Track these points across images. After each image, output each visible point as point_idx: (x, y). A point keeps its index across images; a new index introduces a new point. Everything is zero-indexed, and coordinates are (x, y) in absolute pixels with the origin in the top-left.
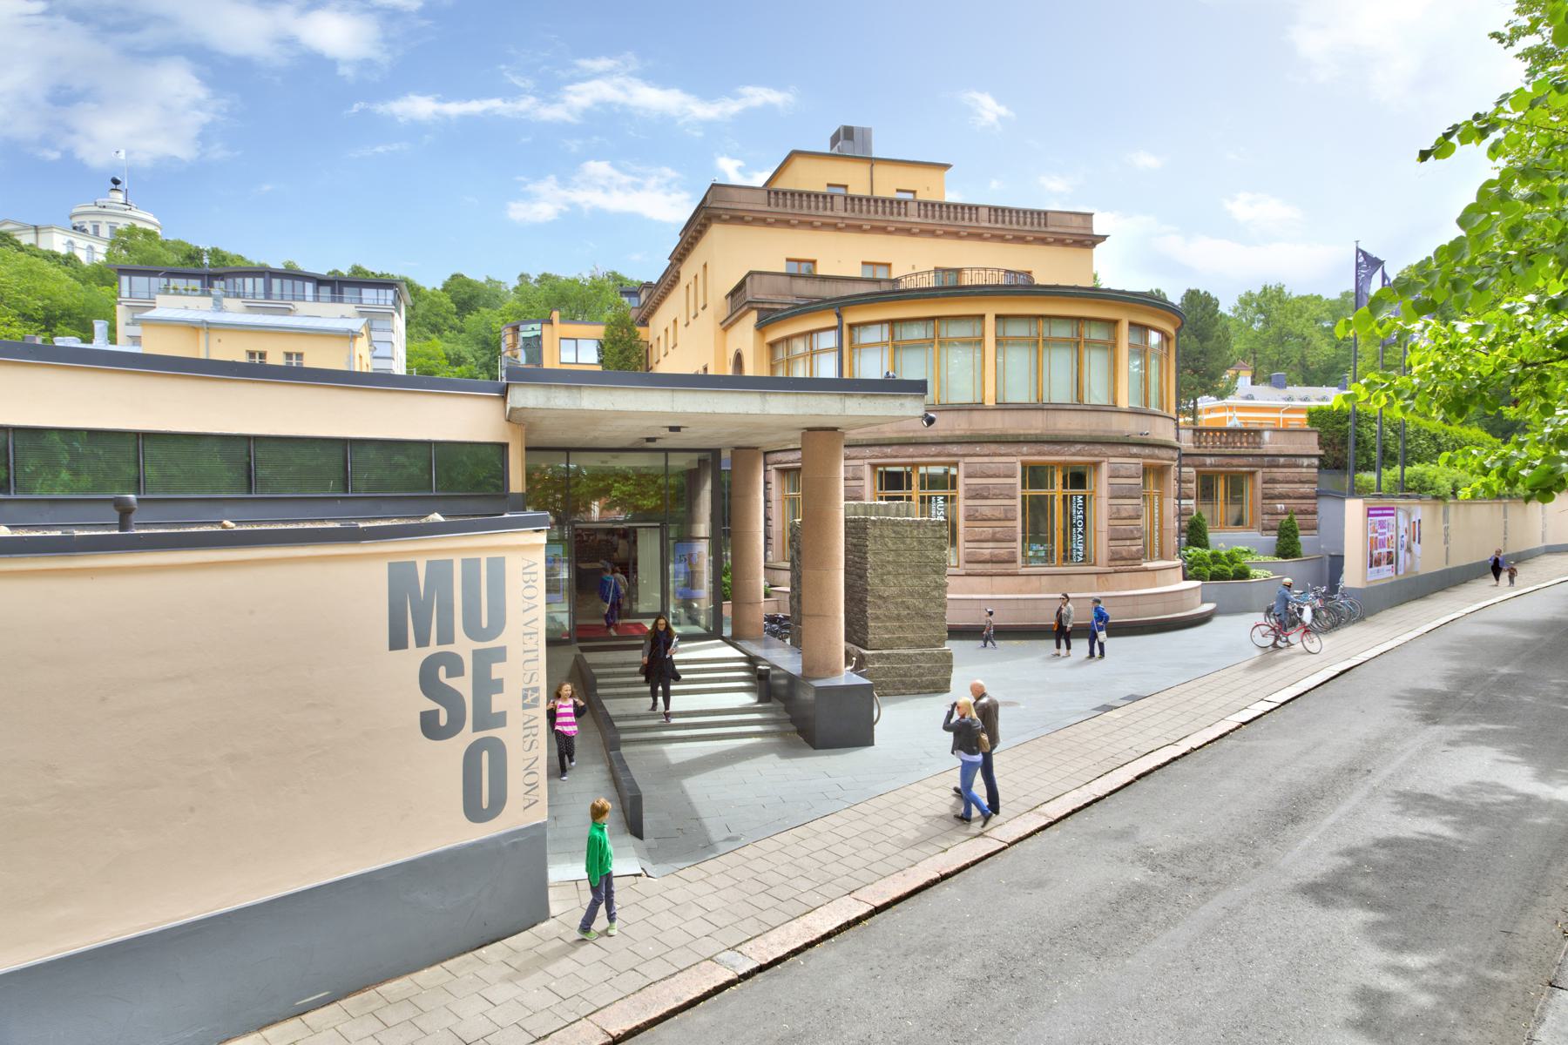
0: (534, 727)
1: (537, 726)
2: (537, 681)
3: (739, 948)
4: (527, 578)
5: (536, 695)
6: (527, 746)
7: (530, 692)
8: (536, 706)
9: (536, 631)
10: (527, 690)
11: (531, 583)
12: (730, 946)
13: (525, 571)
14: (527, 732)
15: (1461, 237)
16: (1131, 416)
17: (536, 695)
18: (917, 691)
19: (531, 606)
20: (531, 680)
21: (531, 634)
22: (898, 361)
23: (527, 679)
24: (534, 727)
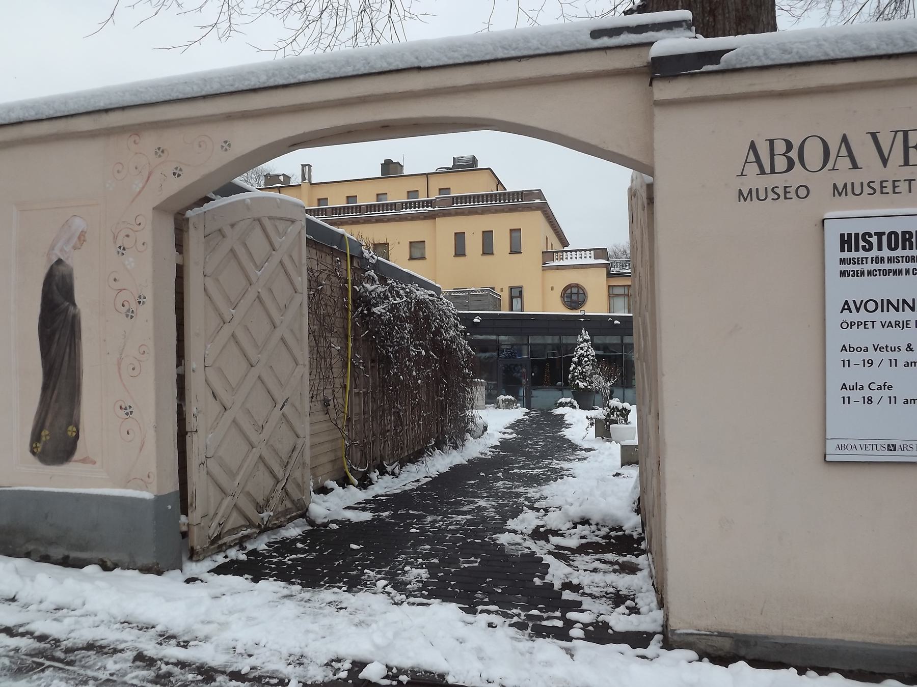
1: (771, 142)
4: (781, 163)
9: (900, 136)
11: (794, 154)
13: (767, 169)
19: (844, 151)
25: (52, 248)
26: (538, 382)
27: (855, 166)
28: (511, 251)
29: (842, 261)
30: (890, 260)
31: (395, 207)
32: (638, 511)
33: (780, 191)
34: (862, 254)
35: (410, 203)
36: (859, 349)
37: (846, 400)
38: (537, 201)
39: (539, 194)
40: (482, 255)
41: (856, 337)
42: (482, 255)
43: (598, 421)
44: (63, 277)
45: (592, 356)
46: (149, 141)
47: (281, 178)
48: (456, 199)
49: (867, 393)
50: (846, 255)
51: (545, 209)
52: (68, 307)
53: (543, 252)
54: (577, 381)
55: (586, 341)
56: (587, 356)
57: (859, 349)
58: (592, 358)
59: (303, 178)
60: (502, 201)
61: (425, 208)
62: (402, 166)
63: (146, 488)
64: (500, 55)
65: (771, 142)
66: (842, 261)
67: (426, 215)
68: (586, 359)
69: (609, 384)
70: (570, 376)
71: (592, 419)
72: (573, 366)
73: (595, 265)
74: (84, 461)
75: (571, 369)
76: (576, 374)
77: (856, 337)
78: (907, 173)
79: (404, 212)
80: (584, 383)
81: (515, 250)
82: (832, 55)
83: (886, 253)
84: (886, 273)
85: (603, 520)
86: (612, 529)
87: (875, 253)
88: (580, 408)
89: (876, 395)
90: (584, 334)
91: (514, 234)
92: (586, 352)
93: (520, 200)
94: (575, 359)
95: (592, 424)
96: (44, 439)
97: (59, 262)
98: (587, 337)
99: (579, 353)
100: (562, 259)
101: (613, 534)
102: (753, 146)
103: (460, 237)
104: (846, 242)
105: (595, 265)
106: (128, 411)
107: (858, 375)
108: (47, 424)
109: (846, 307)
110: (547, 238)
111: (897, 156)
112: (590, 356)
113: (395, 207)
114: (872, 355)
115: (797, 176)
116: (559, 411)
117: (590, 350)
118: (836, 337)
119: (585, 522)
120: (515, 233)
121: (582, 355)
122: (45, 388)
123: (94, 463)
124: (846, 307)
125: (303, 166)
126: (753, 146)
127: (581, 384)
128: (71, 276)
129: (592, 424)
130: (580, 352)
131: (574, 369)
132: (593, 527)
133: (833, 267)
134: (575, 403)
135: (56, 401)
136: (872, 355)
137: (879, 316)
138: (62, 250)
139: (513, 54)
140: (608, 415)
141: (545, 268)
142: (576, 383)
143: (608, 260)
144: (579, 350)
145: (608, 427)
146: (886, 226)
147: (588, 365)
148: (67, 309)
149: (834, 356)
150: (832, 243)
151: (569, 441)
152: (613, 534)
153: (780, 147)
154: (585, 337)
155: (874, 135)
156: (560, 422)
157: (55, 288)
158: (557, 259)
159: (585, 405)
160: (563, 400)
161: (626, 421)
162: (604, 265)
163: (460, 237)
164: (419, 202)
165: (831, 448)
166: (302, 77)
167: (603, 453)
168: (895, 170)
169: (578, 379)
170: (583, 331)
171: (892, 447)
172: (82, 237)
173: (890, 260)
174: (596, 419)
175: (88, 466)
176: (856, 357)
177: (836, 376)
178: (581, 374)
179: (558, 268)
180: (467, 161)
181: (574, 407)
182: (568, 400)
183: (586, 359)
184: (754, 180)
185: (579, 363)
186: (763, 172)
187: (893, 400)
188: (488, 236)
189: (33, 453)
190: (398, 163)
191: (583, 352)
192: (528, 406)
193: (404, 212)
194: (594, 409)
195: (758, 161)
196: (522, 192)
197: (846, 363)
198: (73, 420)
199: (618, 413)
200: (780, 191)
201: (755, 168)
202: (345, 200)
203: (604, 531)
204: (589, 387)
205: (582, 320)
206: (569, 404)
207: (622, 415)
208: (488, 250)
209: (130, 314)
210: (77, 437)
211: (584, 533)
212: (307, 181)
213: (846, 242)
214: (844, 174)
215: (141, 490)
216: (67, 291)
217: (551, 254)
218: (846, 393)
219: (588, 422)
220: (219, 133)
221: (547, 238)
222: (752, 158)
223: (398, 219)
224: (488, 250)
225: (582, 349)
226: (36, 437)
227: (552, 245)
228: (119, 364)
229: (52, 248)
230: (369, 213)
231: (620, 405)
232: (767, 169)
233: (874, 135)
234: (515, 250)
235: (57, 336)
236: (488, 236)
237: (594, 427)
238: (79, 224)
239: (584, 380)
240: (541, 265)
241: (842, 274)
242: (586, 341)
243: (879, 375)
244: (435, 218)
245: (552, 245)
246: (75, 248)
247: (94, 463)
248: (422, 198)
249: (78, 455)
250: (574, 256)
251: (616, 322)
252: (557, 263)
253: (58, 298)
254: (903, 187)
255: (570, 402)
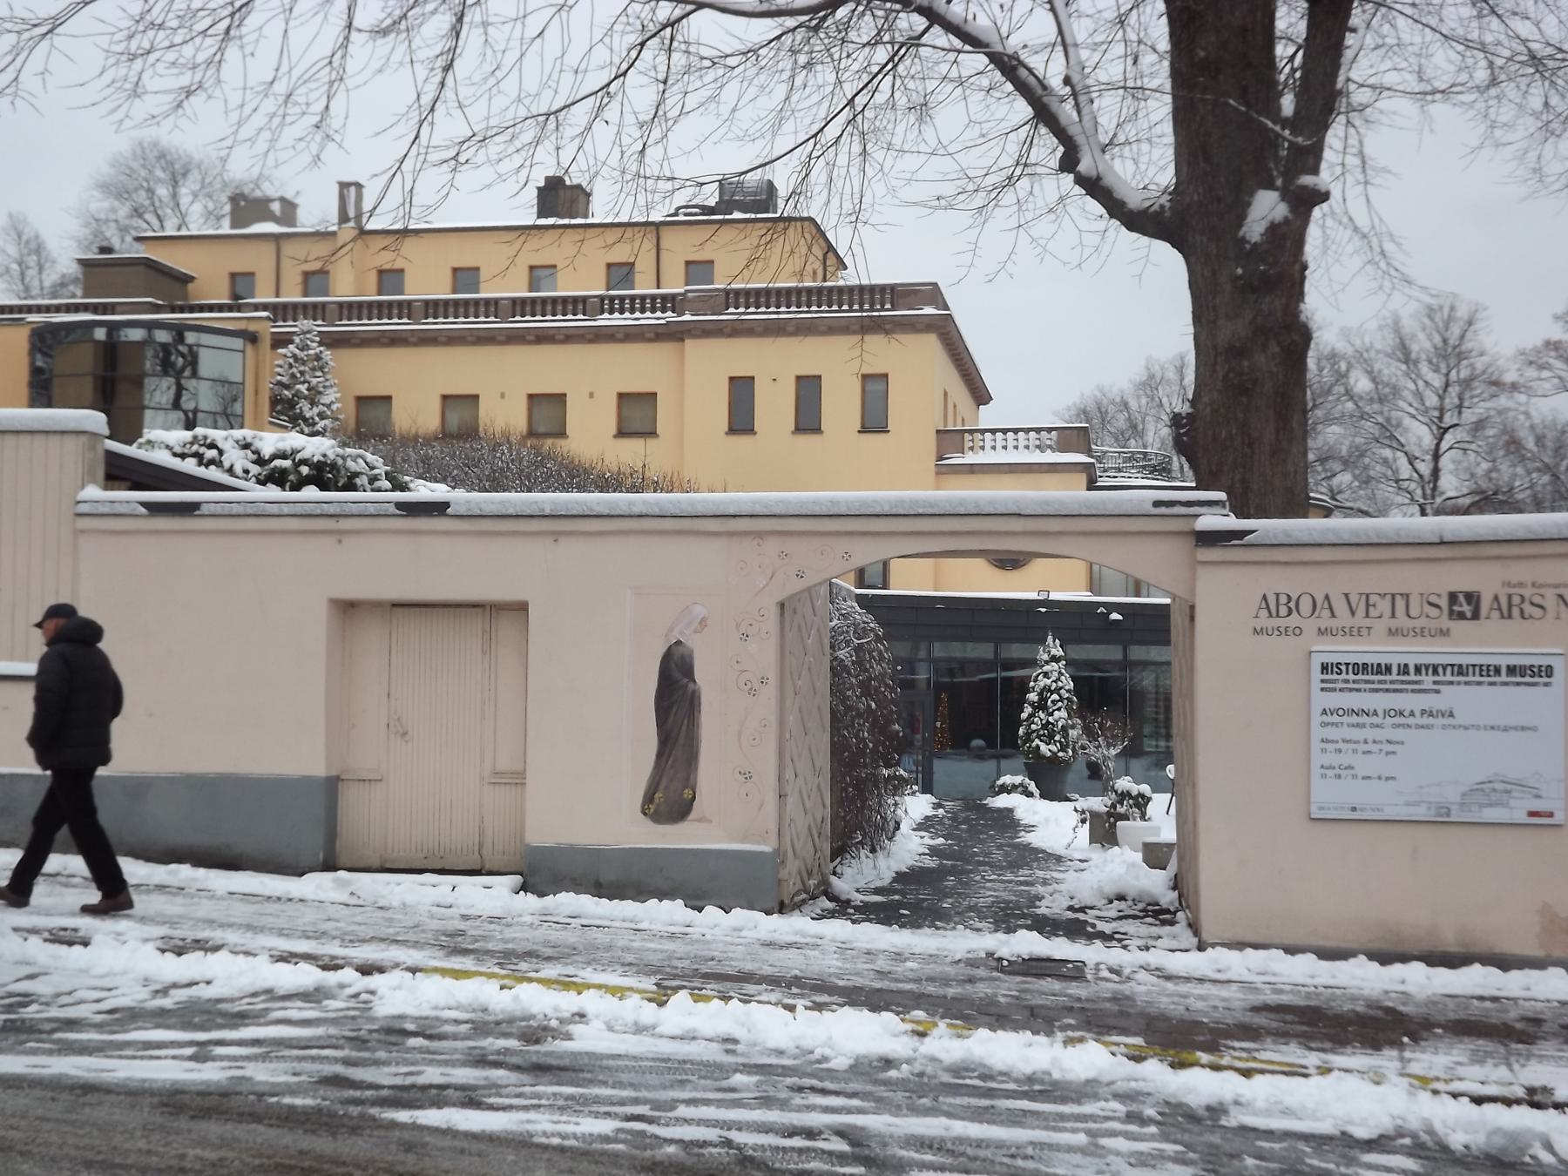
0: (1277, 600)
1: (1277, 595)
2: (1439, 595)
3: (685, 111)
4: (1283, 611)
5: (1461, 598)
6: (1537, 612)
7: (1456, 608)
8: (1479, 598)
9: (1364, 597)
10: (1451, 612)
11: (1292, 605)
12: (648, 151)
13: (1274, 614)
14: (1516, 612)
15: (105, 758)
16: (1267, 941)
17: (1461, 598)
18: (982, 1153)
19: (1326, 605)
20: (1437, 606)
21: (1368, 605)
22: (402, 839)
23: (1434, 612)
24: (1277, 600)
25: (671, 630)
26: (958, 741)
27: (1333, 615)
28: (863, 427)
29: (1322, 681)
30: (1354, 682)
31: (584, 308)
32: (1174, 888)
33: (1282, 630)
34: (1335, 676)
35: (612, 299)
36: (1332, 742)
37: (1324, 776)
38: (929, 310)
39: (933, 294)
40: (793, 433)
41: (1330, 733)
42: (793, 433)
43: (1095, 816)
44: (683, 657)
45: (1068, 691)
46: (772, 546)
47: (276, 207)
48: (733, 297)
49: (1337, 771)
50: (1325, 677)
51: (947, 333)
52: (687, 684)
53: (938, 431)
54: (1037, 741)
55: (1055, 659)
56: (1058, 690)
57: (1332, 742)
58: (1067, 695)
59: (344, 218)
60: (845, 307)
61: (658, 314)
62: (589, 195)
63: (764, 841)
64: (1084, 512)
65: (1277, 595)
66: (1322, 681)
67: (660, 330)
68: (1055, 697)
69: (1113, 752)
70: (1021, 731)
71: (1083, 812)
72: (1028, 710)
73: (1059, 467)
74: (700, 820)
75: (1024, 715)
76: (1034, 727)
77: (1330, 733)
78: (1367, 622)
79: (605, 320)
80: (1050, 747)
81: (874, 422)
82: (1320, 541)
83: (1351, 677)
84: (1351, 690)
85: (1140, 896)
86: (1149, 904)
87: (1343, 676)
88: (1043, 796)
89: (1343, 773)
90: (1051, 644)
91: (871, 386)
92: (1055, 681)
93: (888, 306)
94: (1033, 697)
95: (1083, 821)
96: (657, 801)
97: (679, 643)
98: (1058, 652)
99: (1042, 684)
100: (983, 448)
101: (1150, 908)
102: (1265, 597)
103: (741, 390)
104: (1325, 668)
105: (1059, 467)
106: (747, 776)
107: (1332, 759)
108: (662, 787)
109: (1324, 712)
110: (946, 394)
111: (1361, 611)
112: (1062, 691)
113: (584, 308)
114: (1341, 745)
115: (1294, 620)
116: (1002, 801)
117: (1063, 678)
118: (1318, 732)
119: (1121, 898)
120: (874, 388)
121: (1047, 689)
122: (659, 755)
123: (710, 821)
124: (1324, 712)
125: (344, 186)
126: (1265, 597)
127: (1044, 748)
128: (691, 656)
129: (1083, 821)
130: (1043, 682)
131: (1031, 716)
132: (1130, 903)
133: (1316, 685)
134: (1032, 787)
135: (672, 767)
136: (1341, 745)
137: (1346, 719)
138: (681, 633)
139: (1094, 512)
140: (1113, 806)
141: (943, 469)
142: (1034, 744)
143: (1089, 452)
144: (1040, 677)
145: (1113, 826)
146: (1352, 659)
147: (1059, 709)
148: (686, 686)
149: (1316, 746)
150: (1316, 668)
151: (1037, 851)
152: (1150, 908)
153: (1283, 599)
154: (1054, 652)
155: (1346, 595)
156: (1007, 821)
157: (673, 665)
158: (972, 449)
159: (1052, 791)
160: (1007, 779)
161: (1143, 817)
162: (1080, 467)
163: (741, 390)
164: (633, 298)
165: (1314, 808)
166: (921, 511)
167: (1112, 861)
168: (1359, 620)
169: (1039, 737)
170: (1050, 639)
171: (1354, 809)
172: (703, 622)
173: (1354, 682)
174: (1091, 812)
175: (704, 825)
176: (1330, 747)
177: (1318, 759)
178: (1044, 727)
179: (973, 469)
180: (756, 194)
181: (1030, 795)
182: (1018, 779)
183: (1055, 697)
184: (1264, 621)
185: (1041, 705)
186: (1271, 616)
187: (1354, 777)
188: (808, 390)
189: (645, 814)
190: (579, 187)
191: (1048, 682)
192: (927, 789)
193: (605, 320)
194: (1068, 800)
195: (1268, 607)
196: (893, 287)
197: (1324, 751)
198: (689, 782)
199: (1131, 802)
200: (1282, 630)
201: (1264, 613)
202: (446, 278)
203: (1141, 906)
204: (1061, 754)
205: (1043, 610)
206: (1020, 789)
207: (1138, 805)
208: (808, 420)
209: (753, 692)
210: (694, 798)
211: (1121, 908)
212: (352, 224)
213: (1325, 668)
214: (1325, 621)
215: (759, 843)
216: (687, 669)
217: (958, 436)
218: (1323, 771)
219: (1077, 817)
220: (842, 545)
221: (946, 394)
222: (1264, 605)
223: (591, 336)
224: (808, 420)
225: (1046, 675)
226: (649, 798)
227: (955, 406)
228: (740, 735)
229: (671, 630)
230: (517, 318)
231: (1135, 789)
232: (1274, 614)
233: (1346, 595)
234: (874, 422)
235: (674, 709)
236: (808, 390)
237: (1087, 826)
238: (700, 611)
239: (1049, 739)
240: (932, 461)
241: (1322, 689)
242: (1055, 659)
243: (1345, 759)
244: (683, 340)
245: (955, 406)
246: (696, 632)
247: (710, 821)
248: (644, 287)
249: (692, 815)
250: (1011, 443)
251: (1115, 616)
252: (970, 458)
253: (676, 674)
254: (1364, 631)
255: (1021, 785)
